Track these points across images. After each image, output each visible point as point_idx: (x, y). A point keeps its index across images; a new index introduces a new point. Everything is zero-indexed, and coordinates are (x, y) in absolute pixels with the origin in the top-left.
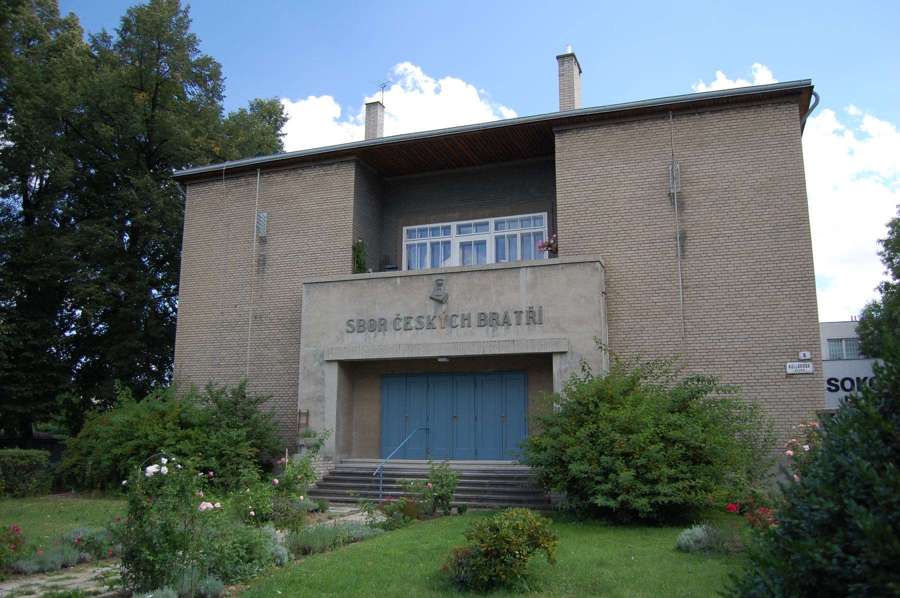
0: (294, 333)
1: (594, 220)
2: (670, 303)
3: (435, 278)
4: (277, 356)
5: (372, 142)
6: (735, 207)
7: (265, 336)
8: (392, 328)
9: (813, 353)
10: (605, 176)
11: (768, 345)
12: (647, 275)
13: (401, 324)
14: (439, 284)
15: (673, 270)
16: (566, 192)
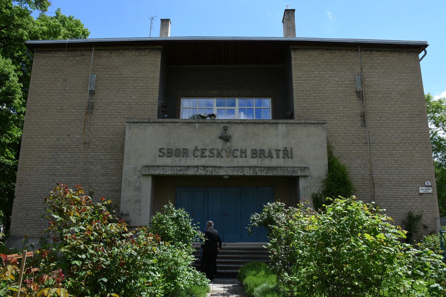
0: (113, 155)
1: (315, 101)
2: (359, 151)
3: (222, 126)
4: (100, 171)
5: (164, 38)
6: (390, 102)
7: (91, 157)
8: (192, 155)
9: (432, 182)
10: (321, 77)
11: (410, 177)
12: (345, 135)
13: (199, 153)
14: (225, 129)
15: (360, 133)
16: (298, 83)
